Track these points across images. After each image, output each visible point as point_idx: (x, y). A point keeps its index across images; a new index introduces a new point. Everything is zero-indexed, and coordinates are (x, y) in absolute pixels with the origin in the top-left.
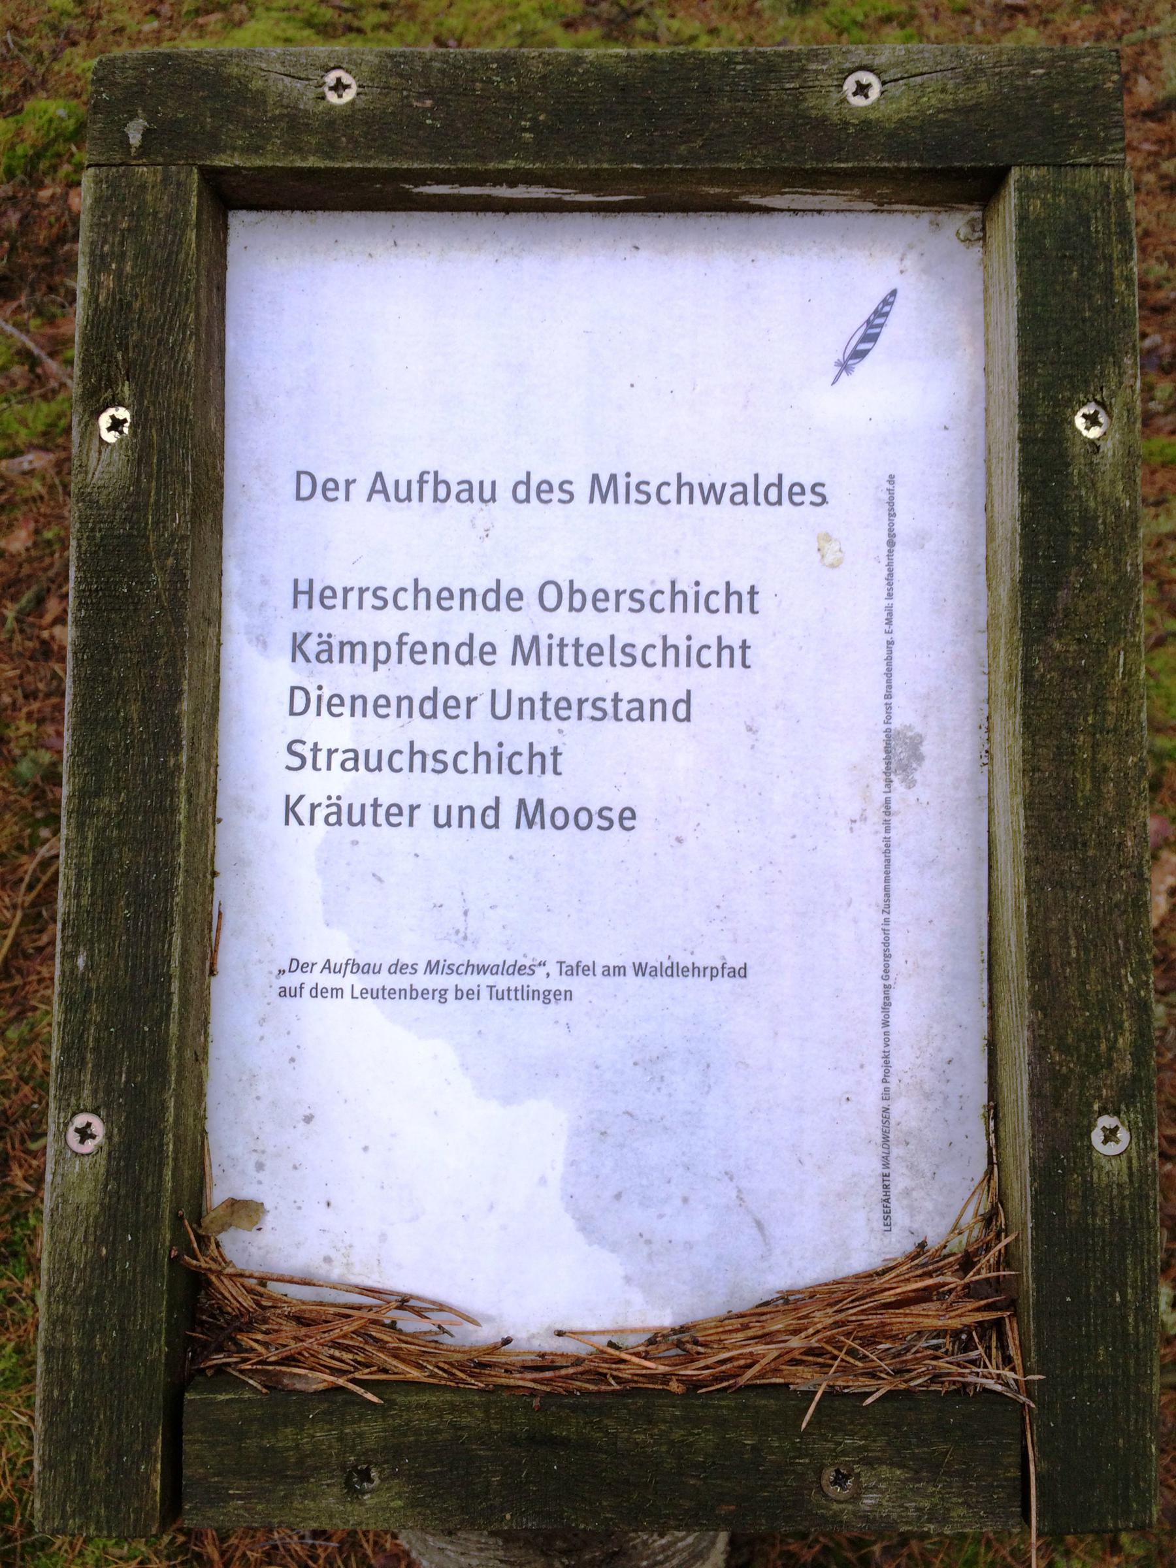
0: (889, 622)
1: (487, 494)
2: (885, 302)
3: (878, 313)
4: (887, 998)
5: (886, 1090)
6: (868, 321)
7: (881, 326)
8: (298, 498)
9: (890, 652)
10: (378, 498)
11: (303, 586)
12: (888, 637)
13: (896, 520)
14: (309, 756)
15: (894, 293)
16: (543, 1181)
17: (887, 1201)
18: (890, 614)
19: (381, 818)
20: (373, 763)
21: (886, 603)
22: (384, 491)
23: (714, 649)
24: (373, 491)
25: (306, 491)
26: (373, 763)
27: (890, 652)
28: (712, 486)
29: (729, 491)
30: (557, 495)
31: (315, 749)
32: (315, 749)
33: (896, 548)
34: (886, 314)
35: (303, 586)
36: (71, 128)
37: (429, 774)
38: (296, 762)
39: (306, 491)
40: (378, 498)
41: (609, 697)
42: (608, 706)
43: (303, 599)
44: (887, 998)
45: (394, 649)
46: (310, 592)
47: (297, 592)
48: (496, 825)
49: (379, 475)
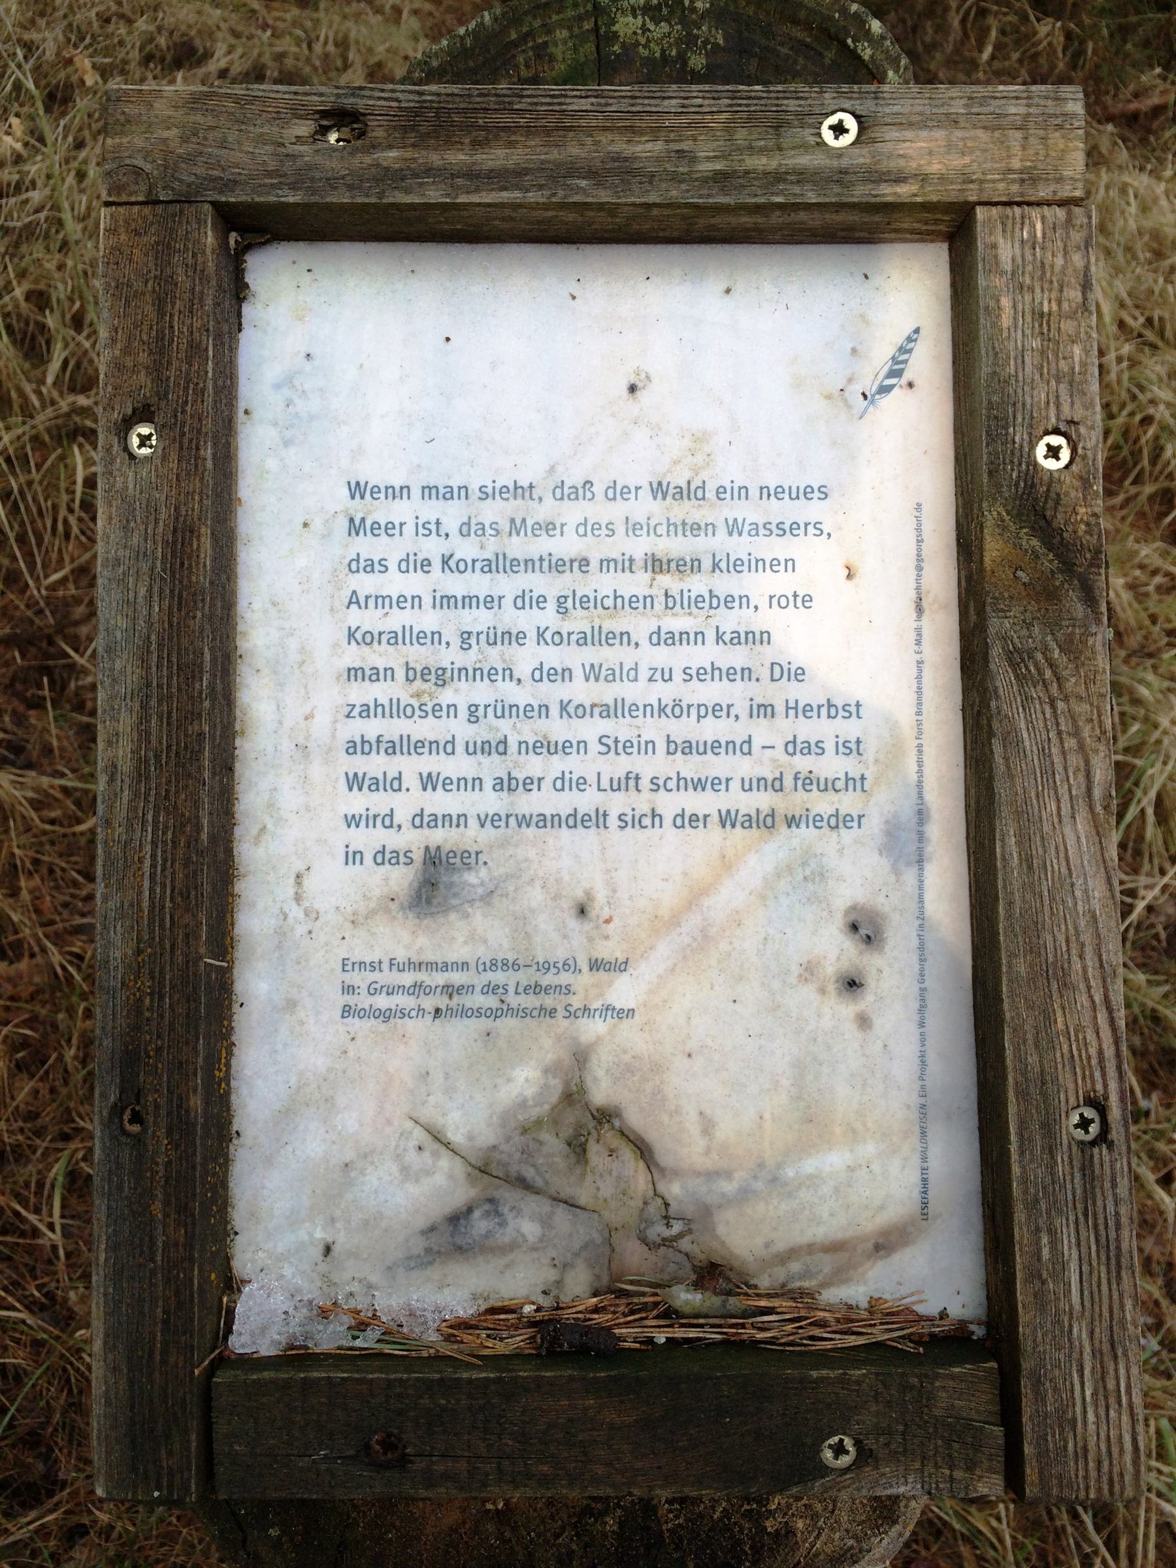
0: (918, 643)
1: (523, 746)
2: (909, 339)
3: (902, 350)
4: (923, 1000)
5: (923, 1087)
6: (893, 358)
7: (906, 362)
8: (773, 680)
9: (920, 671)
10: (354, 607)
11: (792, 704)
12: (918, 657)
13: (927, 965)
14: (613, 746)
15: (917, 331)
16: (900, 1284)
17: (925, 1192)
18: (919, 635)
19: (799, 603)
20: (701, 749)
21: (915, 625)
22: (358, 603)
23: (665, 527)
24: (350, 603)
25: (777, 675)
26: (701, 749)
27: (920, 671)
28: (430, 775)
29: (535, 819)
30: (817, 494)
31: (616, 741)
32: (616, 741)
33: (900, 340)
34: (910, 351)
35: (792, 704)
36: (795, 637)
37: (813, 756)
38: (604, 749)
39: (777, 675)
40: (354, 607)
41: (854, 740)
42: (433, 527)
43: (792, 712)
44: (923, 1000)
45: (791, 599)
46: (796, 708)
47: (788, 708)
48: (636, 680)
49: (354, 592)
